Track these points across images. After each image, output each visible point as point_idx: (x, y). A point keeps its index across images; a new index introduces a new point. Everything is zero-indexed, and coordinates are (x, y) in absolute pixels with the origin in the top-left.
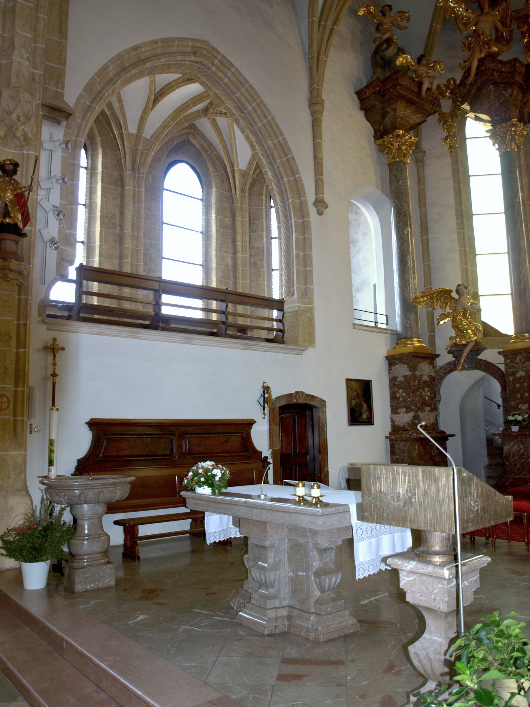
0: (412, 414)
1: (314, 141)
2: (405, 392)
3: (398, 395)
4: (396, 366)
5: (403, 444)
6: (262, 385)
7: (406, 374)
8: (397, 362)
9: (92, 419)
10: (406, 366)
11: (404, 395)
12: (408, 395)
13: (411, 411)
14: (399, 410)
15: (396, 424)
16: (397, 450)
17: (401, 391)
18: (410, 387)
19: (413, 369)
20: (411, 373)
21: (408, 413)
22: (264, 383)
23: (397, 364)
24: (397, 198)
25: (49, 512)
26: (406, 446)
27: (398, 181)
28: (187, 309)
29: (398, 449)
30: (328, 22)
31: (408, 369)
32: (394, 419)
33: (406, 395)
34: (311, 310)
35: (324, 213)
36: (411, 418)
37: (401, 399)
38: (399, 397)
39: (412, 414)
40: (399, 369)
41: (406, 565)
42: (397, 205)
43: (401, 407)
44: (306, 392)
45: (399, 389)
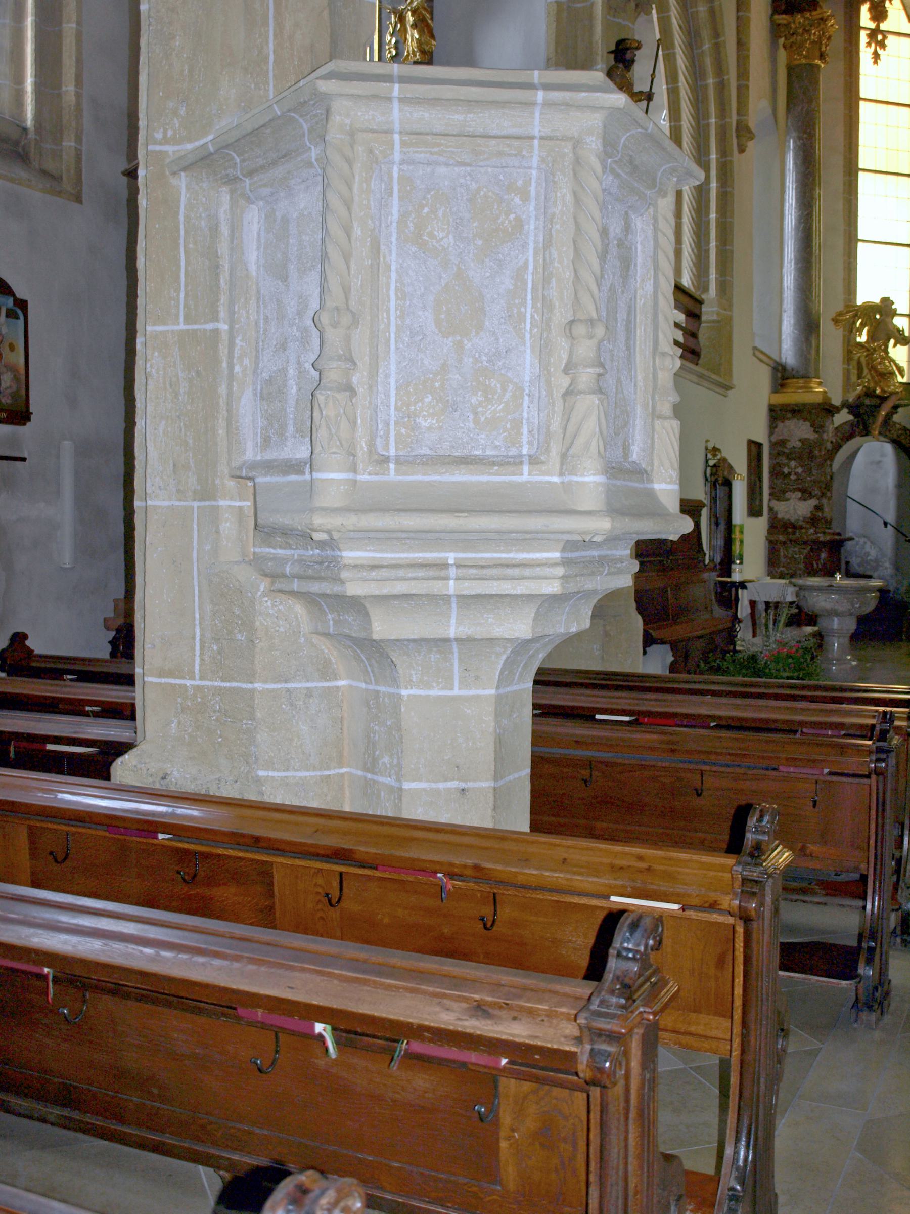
0: (813, 502)
1: (738, 10)
2: (802, 467)
3: (786, 470)
4: (787, 423)
5: (796, 549)
6: (703, 445)
7: (806, 436)
8: (789, 415)
9: (24, 424)
10: (808, 424)
11: (800, 470)
12: (809, 471)
13: (811, 496)
14: (788, 495)
15: (780, 516)
16: (783, 560)
17: (793, 464)
18: (811, 457)
19: (818, 428)
20: (817, 435)
21: (805, 500)
22: (707, 441)
23: (788, 419)
24: (805, 132)
25: (775, 1059)
26: (800, 553)
27: (810, 101)
28: (900, 172)
29: (785, 557)
30: (536, 81)
31: (812, 429)
32: (775, 509)
33: (804, 471)
34: (730, 319)
35: (747, 149)
36: (811, 509)
37: (793, 477)
38: (789, 474)
39: (813, 502)
40: (792, 427)
41: (559, 619)
42: (804, 145)
43: (794, 491)
44: (729, 461)
45: (790, 459)
